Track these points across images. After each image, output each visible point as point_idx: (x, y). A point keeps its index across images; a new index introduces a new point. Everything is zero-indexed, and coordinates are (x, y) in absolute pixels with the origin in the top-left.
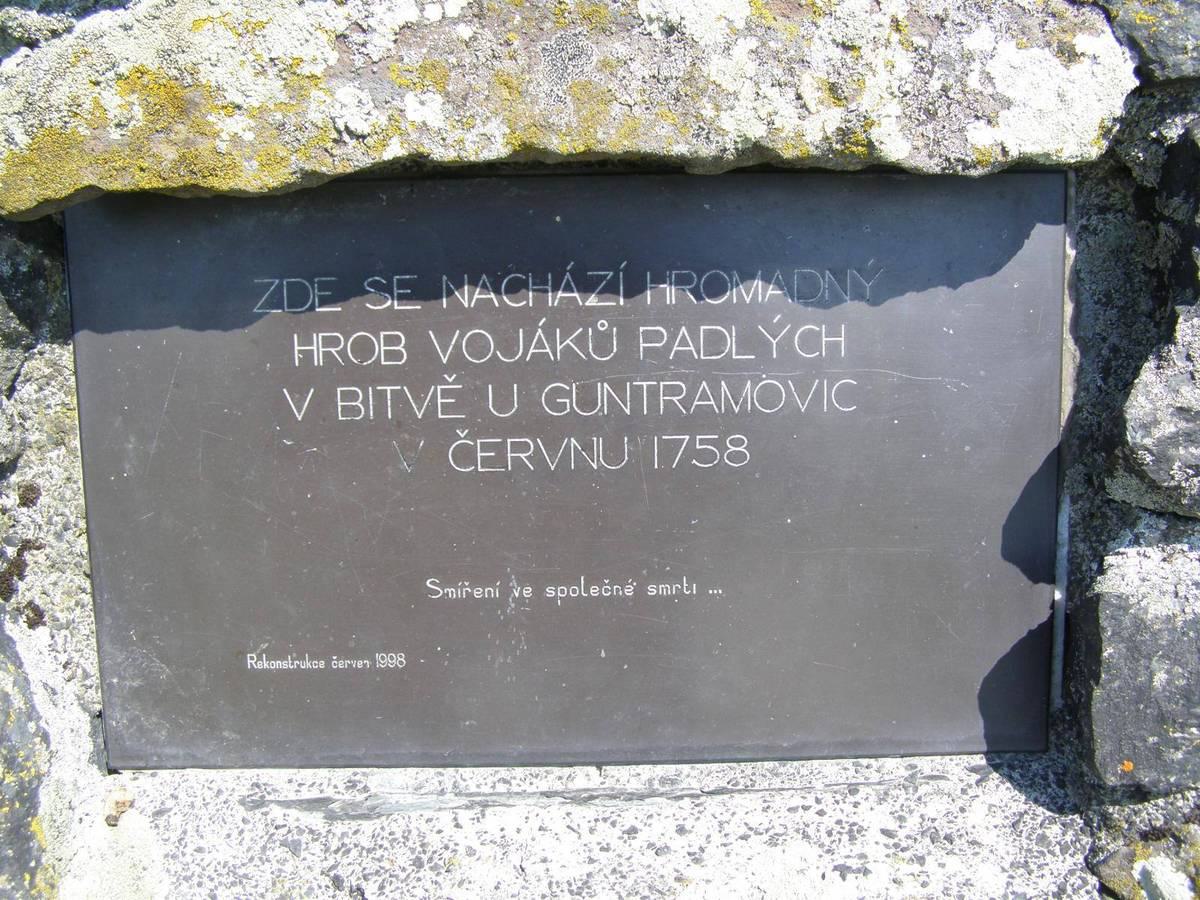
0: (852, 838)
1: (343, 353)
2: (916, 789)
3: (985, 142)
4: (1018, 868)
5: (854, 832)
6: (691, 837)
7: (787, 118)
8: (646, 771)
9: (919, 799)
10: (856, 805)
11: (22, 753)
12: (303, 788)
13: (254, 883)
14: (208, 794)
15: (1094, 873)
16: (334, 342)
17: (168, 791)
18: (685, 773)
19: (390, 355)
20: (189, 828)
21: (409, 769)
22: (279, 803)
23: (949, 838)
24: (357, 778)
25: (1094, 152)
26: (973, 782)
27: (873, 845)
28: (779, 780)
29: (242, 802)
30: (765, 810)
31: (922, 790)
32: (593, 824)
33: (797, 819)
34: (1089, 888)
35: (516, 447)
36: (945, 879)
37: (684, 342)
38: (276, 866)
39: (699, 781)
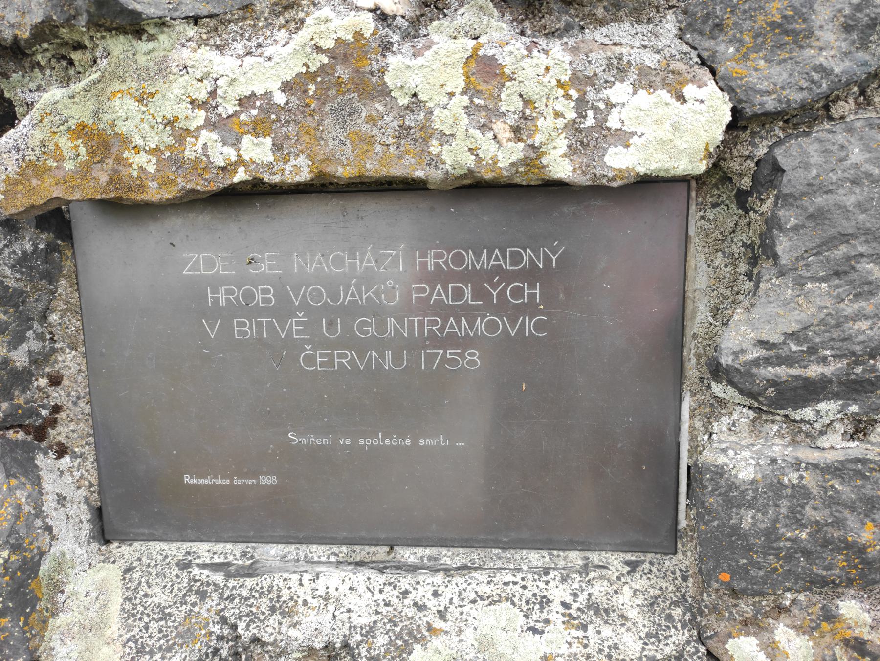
0: (542, 609)
1: (237, 299)
2: (587, 575)
3: (620, 161)
4: (651, 637)
5: (544, 602)
6: (441, 599)
7: (488, 149)
8: (420, 551)
9: (589, 581)
10: (547, 583)
11: (27, 541)
12: (216, 557)
13: (173, 619)
14: (160, 558)
15: (703, 644)
16: (231, 292)
17: (137, 555)
18: (444, 553)
19: (265, 300)
20: (143, 580)
21: (280, 546)
22: (198, 565)
23: (606, 611)
24: (248, 550)
25: (702, 167)
26: (625, 572)
27: (555, 613)
28: (500, 562)
29: (177, 565)
30: (489, 583)
31: (592, 575)
32: (382, 587)
33: (508, 591)
34: (700, 654)
35: (341, 356)
36: (600, 642)
37: (439, 294)
38: (189, 607)
39: (452, 560)
